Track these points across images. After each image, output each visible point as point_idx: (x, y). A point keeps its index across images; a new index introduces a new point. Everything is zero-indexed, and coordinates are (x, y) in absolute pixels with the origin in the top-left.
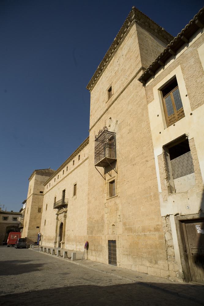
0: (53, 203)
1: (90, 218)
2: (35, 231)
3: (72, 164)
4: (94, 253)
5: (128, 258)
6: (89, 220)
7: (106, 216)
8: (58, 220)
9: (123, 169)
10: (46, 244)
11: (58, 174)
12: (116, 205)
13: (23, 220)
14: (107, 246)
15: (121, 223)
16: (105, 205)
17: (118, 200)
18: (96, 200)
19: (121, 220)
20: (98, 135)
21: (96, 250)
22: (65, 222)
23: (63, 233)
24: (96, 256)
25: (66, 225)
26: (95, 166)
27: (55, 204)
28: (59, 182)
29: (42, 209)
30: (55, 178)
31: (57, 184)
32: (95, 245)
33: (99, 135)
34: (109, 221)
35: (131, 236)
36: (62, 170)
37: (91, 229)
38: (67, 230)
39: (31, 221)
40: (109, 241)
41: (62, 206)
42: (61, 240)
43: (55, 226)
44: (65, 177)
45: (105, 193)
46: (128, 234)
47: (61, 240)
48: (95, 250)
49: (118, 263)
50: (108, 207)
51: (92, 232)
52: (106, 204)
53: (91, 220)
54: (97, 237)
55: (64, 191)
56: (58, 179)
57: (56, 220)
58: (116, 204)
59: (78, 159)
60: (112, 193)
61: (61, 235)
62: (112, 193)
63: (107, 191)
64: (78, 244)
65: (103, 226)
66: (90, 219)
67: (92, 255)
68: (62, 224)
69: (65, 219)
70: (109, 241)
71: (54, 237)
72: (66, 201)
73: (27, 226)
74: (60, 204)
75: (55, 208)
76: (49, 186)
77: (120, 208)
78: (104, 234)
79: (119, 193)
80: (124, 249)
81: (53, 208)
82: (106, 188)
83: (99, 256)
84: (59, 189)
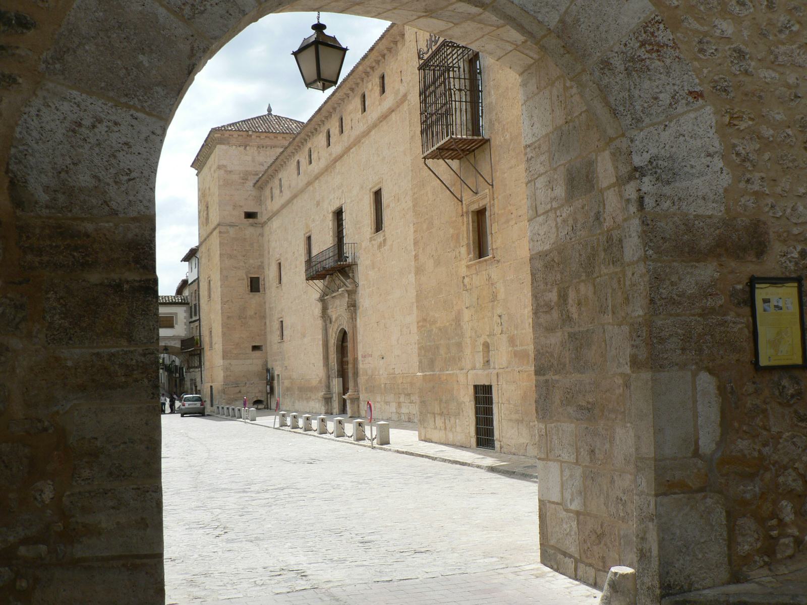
0: (303, 258)
1: (425, 320)
2: (249, 361)
3: (359, 106)
4: (439, 422)
5: (518, 429)
6: (422, 326)
7: (467, 315)
8: (328, 322)
9: (506, 175)
10: (294, 402)
11: (309, 145)
12: (492, 284)
13: (197, 324)
14: (470, 401)
15: (504, 337)
16: (463, 282)
17: (494, 272)
18: (438, 263)
19: (504, 329)
20: (426, 49)
21: (445, 411)
22: (354, 327)
23: (350, 366)
24: (445, 429)
25: (360, 338)
26: (425, 158)
27: (309, 262)
28: (317, 178)
29: (261, 282)
30: (297, 158)
31: (309, 184)
32: (441, 401)
33: (430, 52)
34: (476, 332)
35: (526, 372)
36: (324, 130)
37: (429, 356)
38: (364, 357)
39: (227, 328)
40: (476, 387)
41: (334, 270)
42: (345, 390)
43: (321, 342)
44: (336, 160)
45: (462, 245)
46: (520, 368)
47: (345, 390)
48: (441, 414)
49: (497, 444)
50: (470, 290)
51: (432, 363)
52: (467, 280)
53: (428, 326)
54: (445, 378)
55: (339, 214)
56: (310, 162)
57: (320, 323)
58: (490, 282)
59: (377, 89)
60: (481, 248)
61: (343, 373)
62: (481, 248)
63: (468, 239)
64: (402, 399)
65: (459, 345)
66: (424, 322)
67: (436, 428)
68: (343, 336)
69: (353, 318)
70: (476, 387)
71: (320, 382)
72: (348, 250)
73: (218, 346)
74: (329, 263)
75: (310, 278)
76: (276, 192)
77: (501, 296)
78: (462, 369)
79: (497, 249)
80: (512, 406)
81: (303, 276)
82: (465, 228)
83: (454, 429)
84: (318, 204)
